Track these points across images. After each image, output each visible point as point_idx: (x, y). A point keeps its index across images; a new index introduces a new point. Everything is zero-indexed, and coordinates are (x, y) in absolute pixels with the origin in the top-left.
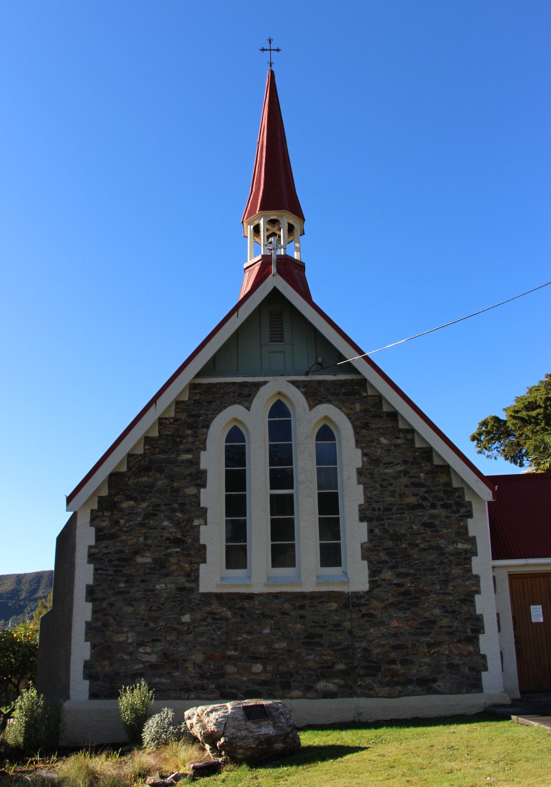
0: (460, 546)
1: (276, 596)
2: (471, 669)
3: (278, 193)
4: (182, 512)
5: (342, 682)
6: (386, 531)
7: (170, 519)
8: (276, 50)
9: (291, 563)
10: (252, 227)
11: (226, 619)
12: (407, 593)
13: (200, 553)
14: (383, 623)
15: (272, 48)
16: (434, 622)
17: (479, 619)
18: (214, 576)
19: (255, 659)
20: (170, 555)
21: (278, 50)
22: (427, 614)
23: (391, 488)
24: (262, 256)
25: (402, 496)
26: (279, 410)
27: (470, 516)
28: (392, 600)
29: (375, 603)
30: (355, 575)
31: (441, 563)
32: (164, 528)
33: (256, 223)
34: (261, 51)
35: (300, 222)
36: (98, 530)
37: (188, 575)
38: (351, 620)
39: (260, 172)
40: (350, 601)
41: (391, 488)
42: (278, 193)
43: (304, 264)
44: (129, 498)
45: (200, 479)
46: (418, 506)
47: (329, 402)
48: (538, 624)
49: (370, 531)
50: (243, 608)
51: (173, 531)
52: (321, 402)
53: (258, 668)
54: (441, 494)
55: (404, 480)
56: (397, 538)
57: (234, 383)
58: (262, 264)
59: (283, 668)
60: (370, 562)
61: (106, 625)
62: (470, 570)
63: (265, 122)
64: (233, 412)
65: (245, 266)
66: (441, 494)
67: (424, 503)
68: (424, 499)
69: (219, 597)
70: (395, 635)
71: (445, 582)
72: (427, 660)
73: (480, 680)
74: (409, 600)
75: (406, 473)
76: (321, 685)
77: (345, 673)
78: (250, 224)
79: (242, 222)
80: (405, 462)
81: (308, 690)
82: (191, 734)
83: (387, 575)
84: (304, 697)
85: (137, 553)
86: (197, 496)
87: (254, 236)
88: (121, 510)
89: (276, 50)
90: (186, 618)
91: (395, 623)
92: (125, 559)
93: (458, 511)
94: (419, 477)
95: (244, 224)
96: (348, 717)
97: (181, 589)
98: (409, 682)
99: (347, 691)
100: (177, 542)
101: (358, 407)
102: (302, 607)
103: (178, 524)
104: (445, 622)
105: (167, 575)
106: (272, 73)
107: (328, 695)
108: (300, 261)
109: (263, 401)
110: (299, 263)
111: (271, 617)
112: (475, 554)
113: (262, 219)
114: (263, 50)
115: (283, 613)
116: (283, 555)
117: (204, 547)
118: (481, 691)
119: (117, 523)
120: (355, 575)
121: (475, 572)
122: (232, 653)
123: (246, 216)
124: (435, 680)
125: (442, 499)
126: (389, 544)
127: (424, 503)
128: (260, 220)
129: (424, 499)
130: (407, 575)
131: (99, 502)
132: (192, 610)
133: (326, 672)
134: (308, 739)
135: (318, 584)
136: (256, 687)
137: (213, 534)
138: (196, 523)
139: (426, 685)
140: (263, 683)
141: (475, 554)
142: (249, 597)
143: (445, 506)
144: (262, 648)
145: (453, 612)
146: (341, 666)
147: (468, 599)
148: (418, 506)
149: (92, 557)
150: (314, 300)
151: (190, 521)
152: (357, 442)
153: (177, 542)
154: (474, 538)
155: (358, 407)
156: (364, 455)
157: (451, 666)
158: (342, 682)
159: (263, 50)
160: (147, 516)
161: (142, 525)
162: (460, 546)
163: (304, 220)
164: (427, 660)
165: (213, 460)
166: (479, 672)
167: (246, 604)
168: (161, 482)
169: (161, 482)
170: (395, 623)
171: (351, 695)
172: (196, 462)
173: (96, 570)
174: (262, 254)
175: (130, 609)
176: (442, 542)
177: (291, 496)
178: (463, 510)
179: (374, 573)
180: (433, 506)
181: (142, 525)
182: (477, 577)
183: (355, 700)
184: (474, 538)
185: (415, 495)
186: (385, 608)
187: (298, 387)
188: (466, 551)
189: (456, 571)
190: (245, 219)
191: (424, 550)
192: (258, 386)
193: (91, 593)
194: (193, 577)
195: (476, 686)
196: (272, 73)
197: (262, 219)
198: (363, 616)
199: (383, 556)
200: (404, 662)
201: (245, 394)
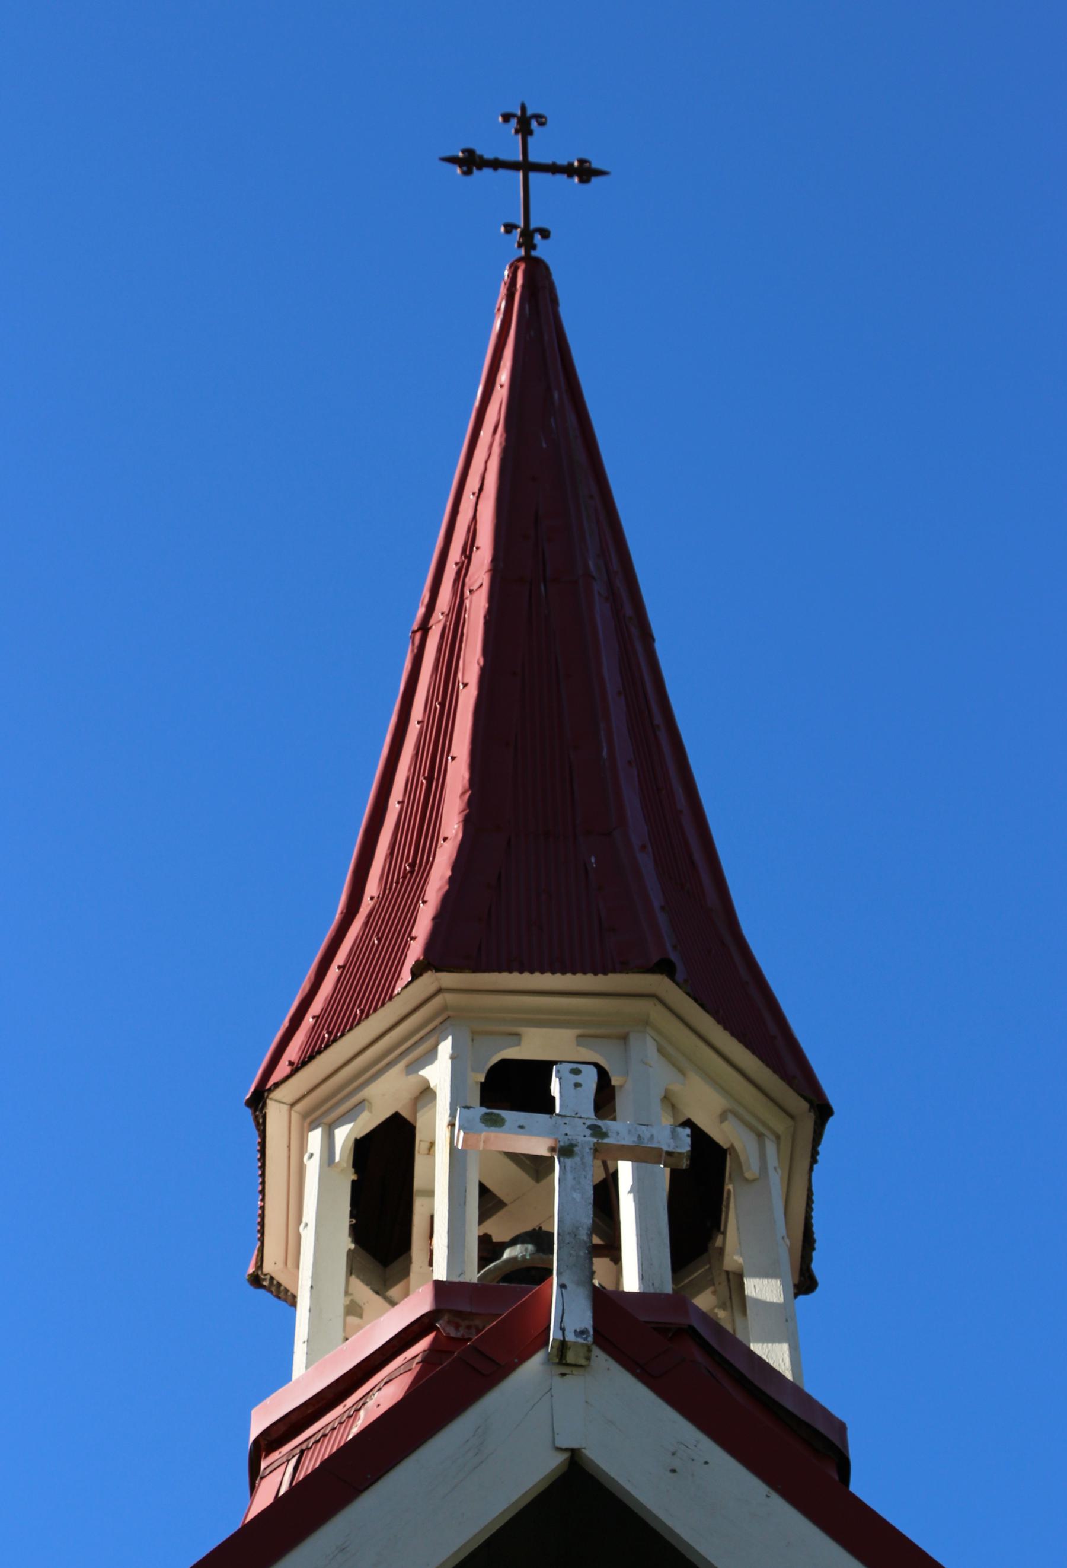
3: (576, 827)
8: (568, 170)
10: (344, 1135)
15: (533, 158)
21: (585, 172)
24: (439, 1286)
33: (385, 1098)
34: (596, 165)
35: (780, 1124)
39: (432, 773)
42: (576, 827)
43: (842, 1428)
58: (429, 1359)
63: (483, 512)
65: (262, 1419)
78: (320, 1114)
79: (258, 1101)
87: (350, 1271)
89: (568, 170)
95: (276, 1113)
106: (537, 293)
108: (794, 1389)
110: (790, 1405)
113: (445, 1048)
114: (470, 162)
123: (293, 1052)
128: (431, 1056)
150: (814, 1175)
159: (470, 162)
163: (823, 1111)
174: (440, 1273)
190: (283, 1069)
196: (537, 293)
197: (445, 1048)
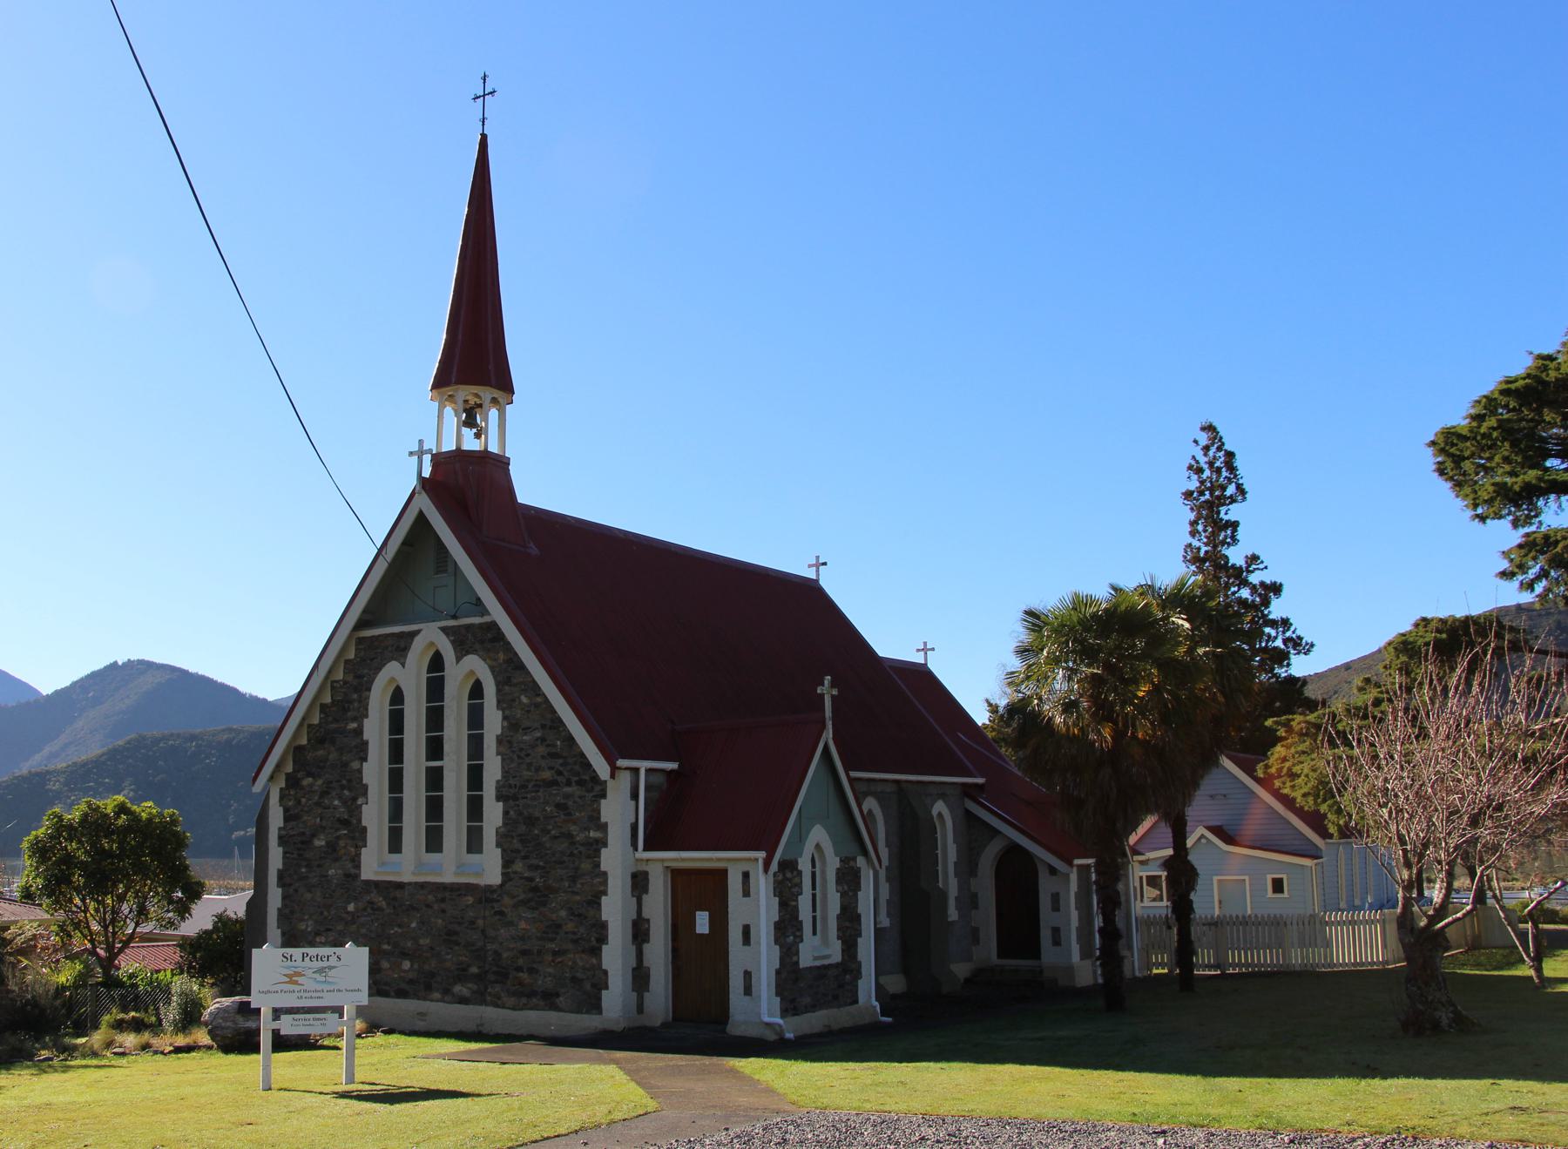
0: (592, 834)
1: (422, 886)
2: (594, 985)
4: (350, 790)
5: (475, 987)
6: (521, 814)
7: (340, 798)
9: (480, 851)
11: (380, 909)
12: (535, 889)
13: (359, 836)
14: (511, 924)
16: (559, 926)
17: (604, 926)
18: (374, 864)
19: (404, 955)
20: (338, 838)
22: (554, 916)
23: (528, 760)
25: (538, 769)
26: (437, 663)
27: (604, 796)
28: (522, 897)
29: (507, 900)
30: (489, 868)
31: (572, 854)
32: (335, 808)
36: (286, 810)
37: (353, 860)
38: (484, 918)
40: (485, 895)
41: (528, 760)
44: (309, 774)
45: (362, 751)
46: (554, 783)
47: (474, 652)
48: (702, 935)
49: (506, 813)
50: (395, 899)
51: (342, 812)
52: (468, 653)
53: (406, 965)
54: (577, 768)
55: (541, 750)
56: (531, 821)
57: (393, 635)
59: (426, 967)
60: (504, 851)
61: (292, 912)
62: (598, 865)
64: (391, 670)
66: (577, 768)
67: (560, 779)
68: (560, 773)
69: (377, 884)
70: (522, 938)
71: (574, 879)
72: (550, 970)
73: (600, 999)
74: (538, 897)
75: (543, 740)
76: (457, 989)
77: (479, 978)
80: (543, 726)
81: (447, 994)
82: (82, 1028)
83: (518, 866)
84: (442, 1000)
85: (314, 835)
86: (360, 771)
88: (302, 788)
90: (351, 907)
91: (523, 925)
92: (307, 843)
93: (592, 790)
94: (554, 746)
96: (471, 1027)
97: (347, 876)
98: (532, 994)
99: (479, 998)
100: (345, 823)
101: (501, 656)
102: (443, 900)
103: (345, 803)
104: (570, 926)
105: (336, 860)
107: (463, 1001)
109: (418, 656)
111: (417, 910)
112: (605, 845)
115: (428, 906)
116: (434, 841)
117: (364, 829)
118: (600, 1013)
119: (299, 802)
120: (489, 868)
121: (603, 867)
122: (386, 947)
124: (558, 995)
125: (578, 774)
126: (522, 829)
127: (560, 779)
129: (560, 773)
130: (537, 867)
131: (287, 780)
132: (356, 899)
133: (461, 975)
134: (326, 1042)
135: (456, 874)
136: (403, 986)
137: (374, 815)
138: (359, 802)
139: (549, 1000)
140: (411, 982)
141: (605, 845)
142: (400, 886)
143: (580, 783)
144: (409, 944)
145: (579, 915)
146: (474, 970)
147: (595, 902)
148: (554, 783)
149: (282, 840)
151: (355, 799)
152: (499, 702)
153: (345, 823)
154: (606, 825)
155: (501, 656)
156: (505, 718)
157: (574, 979)
158: (475, 987)
160: (324, 794)
161: (318, 804)
162: (592, 834)
164: (550, 970)
165: (375, 729)
166: (600, 990)
167: (398, 894)
168: (333, 756)
169: (333, 756)
170: (523, 925)
171: (483, 1002)
172: (359, 732)
173: (285, 853)
175: (308, 896)
176: (573, 829)
177: (441, 768)
178: (597, 788)
179: (506, 864)
180: (569, 784)
181: (318, 804)
182: (605, 874)
183: (482, 1008)
184: (606, 825)
185: (551, 768)
186: (515, 906)
187: (447, 635)
188: (597, 841)
189: (586, 866)
191: (556, 837)
192: (418, 632)
193: (281, 875)
194: (356, 861)
195: (595, 1006)
198: (496, 913)
199: (516, 844)
200: (532, 971)
201: (399, 647)
